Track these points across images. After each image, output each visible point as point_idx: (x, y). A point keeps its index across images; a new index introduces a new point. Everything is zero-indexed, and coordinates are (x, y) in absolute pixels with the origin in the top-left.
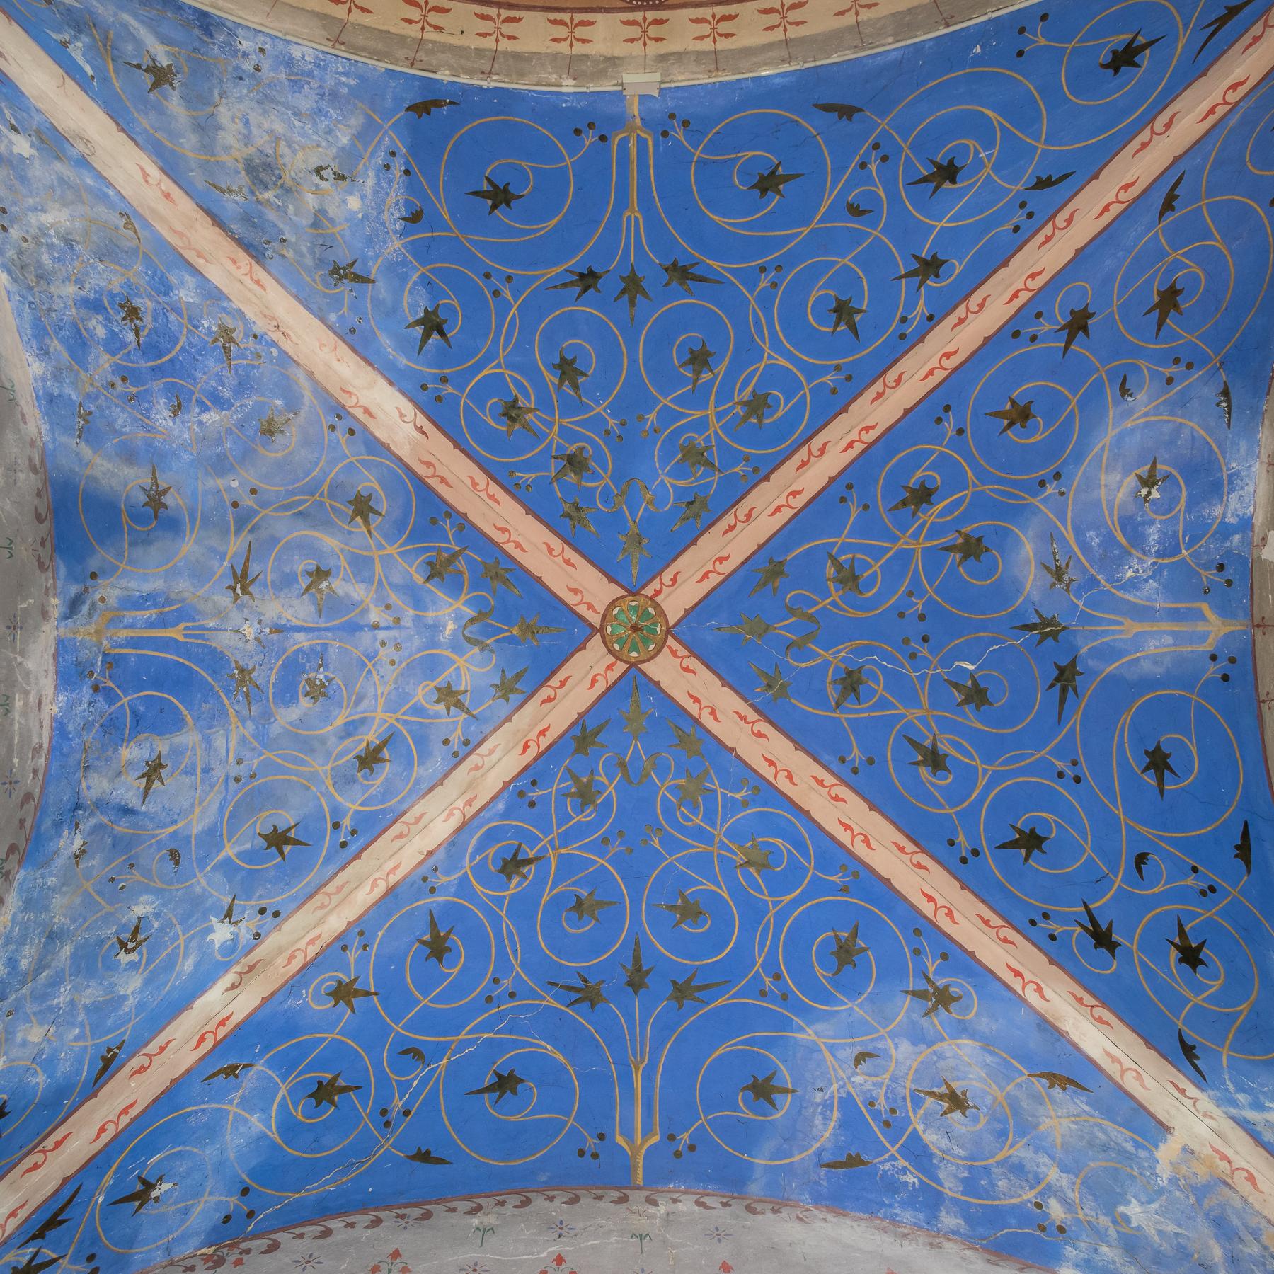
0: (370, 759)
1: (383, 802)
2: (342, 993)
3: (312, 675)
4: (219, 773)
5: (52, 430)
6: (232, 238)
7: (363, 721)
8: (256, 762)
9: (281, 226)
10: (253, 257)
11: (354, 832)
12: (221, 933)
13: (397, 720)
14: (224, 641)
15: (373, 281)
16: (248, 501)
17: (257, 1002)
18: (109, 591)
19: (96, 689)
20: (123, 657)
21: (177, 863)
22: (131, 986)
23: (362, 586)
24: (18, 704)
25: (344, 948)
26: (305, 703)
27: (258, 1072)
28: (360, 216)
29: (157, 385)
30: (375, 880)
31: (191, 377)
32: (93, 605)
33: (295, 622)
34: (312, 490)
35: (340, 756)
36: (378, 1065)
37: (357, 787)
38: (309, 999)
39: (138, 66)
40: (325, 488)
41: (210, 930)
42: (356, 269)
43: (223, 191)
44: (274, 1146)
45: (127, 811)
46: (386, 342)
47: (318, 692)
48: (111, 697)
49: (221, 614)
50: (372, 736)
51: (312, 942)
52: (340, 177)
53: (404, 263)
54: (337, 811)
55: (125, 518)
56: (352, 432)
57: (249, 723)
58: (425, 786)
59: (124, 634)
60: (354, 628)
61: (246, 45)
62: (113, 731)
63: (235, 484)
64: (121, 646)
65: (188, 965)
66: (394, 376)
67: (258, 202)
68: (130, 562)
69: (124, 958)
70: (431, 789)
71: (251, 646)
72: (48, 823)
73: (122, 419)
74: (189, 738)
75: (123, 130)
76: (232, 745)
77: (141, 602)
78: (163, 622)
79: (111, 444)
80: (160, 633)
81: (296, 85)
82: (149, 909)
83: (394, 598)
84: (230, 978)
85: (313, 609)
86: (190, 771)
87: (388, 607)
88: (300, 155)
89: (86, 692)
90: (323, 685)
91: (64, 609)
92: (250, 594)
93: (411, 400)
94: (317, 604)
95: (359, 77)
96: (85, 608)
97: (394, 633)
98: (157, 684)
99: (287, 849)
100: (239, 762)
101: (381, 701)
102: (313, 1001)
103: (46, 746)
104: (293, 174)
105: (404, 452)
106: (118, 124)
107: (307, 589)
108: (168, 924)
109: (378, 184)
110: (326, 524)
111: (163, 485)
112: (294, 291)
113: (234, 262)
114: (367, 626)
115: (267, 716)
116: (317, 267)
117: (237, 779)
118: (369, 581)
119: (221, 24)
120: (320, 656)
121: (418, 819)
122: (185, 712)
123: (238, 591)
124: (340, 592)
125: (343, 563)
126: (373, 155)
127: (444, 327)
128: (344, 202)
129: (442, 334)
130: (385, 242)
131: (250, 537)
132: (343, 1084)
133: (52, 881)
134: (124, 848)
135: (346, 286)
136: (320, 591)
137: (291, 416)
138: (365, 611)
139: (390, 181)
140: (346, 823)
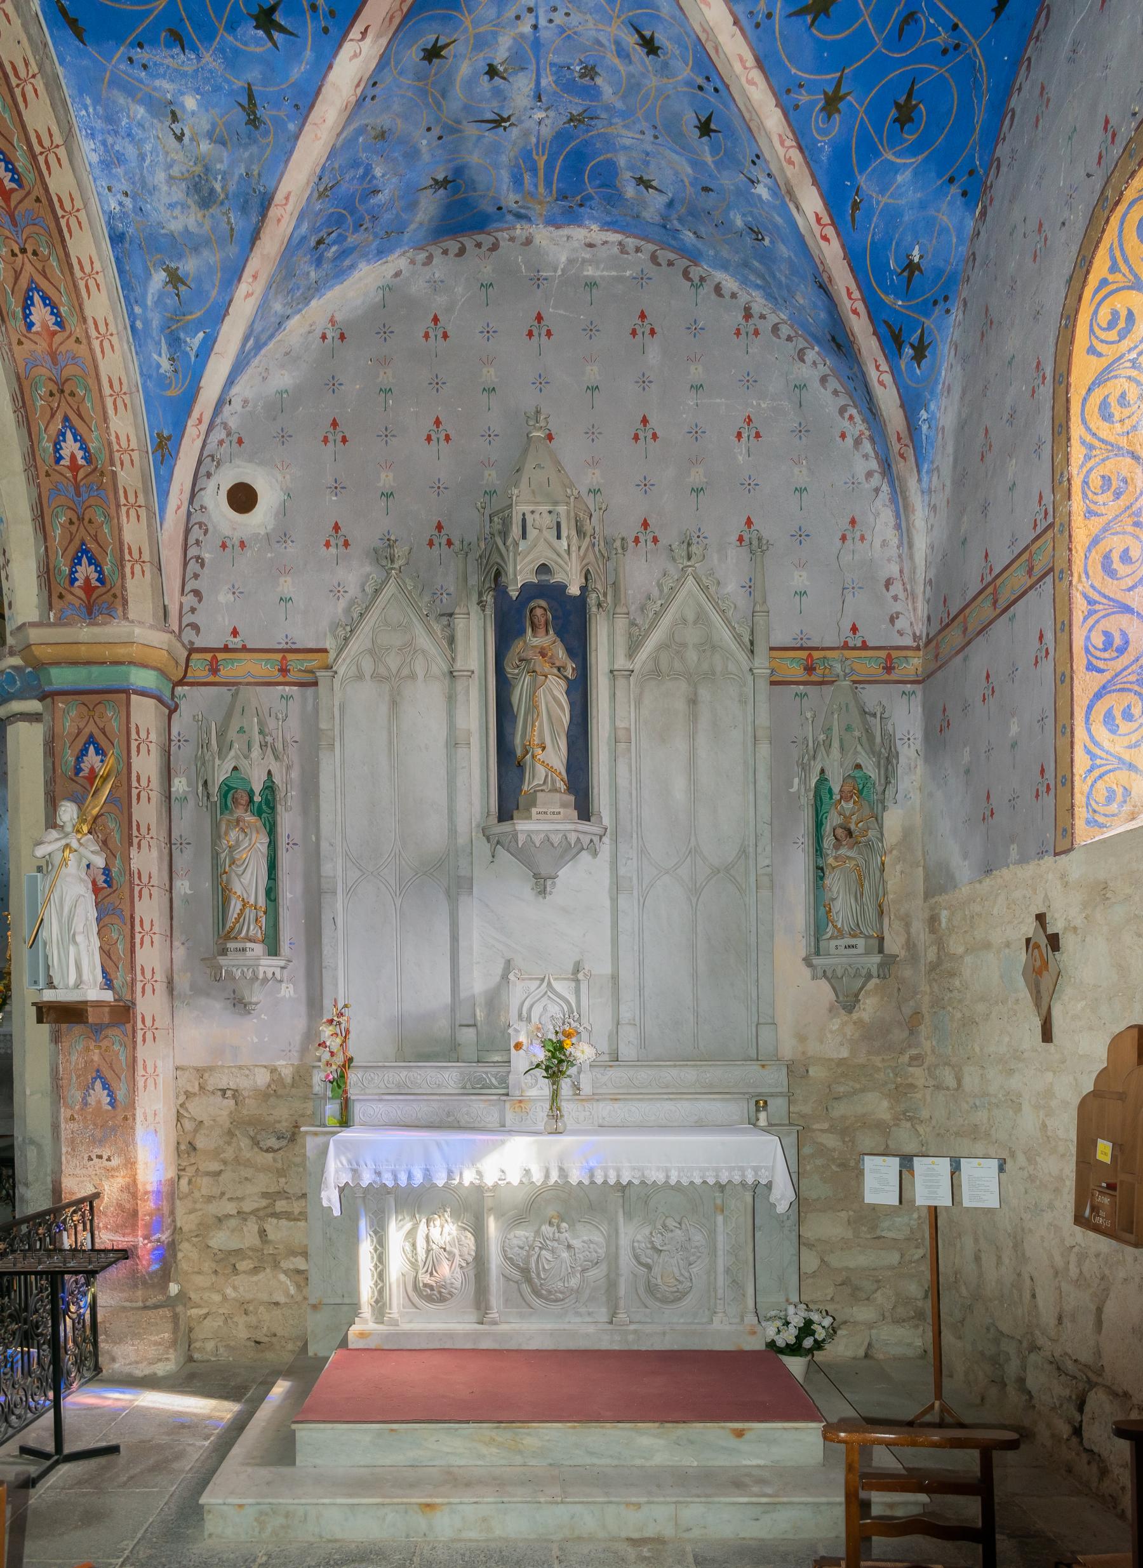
0: (650, 46)
1: (687, 48)
2: (832, 103)
3: (576, 75)
4: (649, 148)
5: (400, 246)
6: (263, 221)
7: (618, 43)
8: (644, 123)
9: (236, 177)
10: (270, 204)
11: (708, 79)
12: (762, 191)
13: (618, 17)
14: (547, 132)
15: (249, 84)
16: (436, 131)
17: (814, 189)
18: (510, 199)
19: (581, 205)
20: (558, 190)
21: (712, 190)
22: (784, 251)
23: (500, 39)
24: (590, 271)
25: (796, 107)
26: (599, 81)
27: (866, 181)
28: (198, 97)
29: (362, 208)
30: (748, 81)
31: (353, 195)
32: (520, 207)
33: (532, 85)
34: (423, 92)
35: (646, 67)
36: (904, 62)
37: (672, 63)
38: (826, 139)
39: (177, 295)
40: (421, 84)
41: (759, 197)
42: (245, 101)
43: (232, 229)
44: (926, 160)
45: (670, 204)
46: (297, 72)
47: (590, 72)
48: (589, 197)
49: (526, 134)
50: (630, 40)
51: (782, 143)
52: (175, 118)
53: (222, 51)
54: (689, 83)
55: (457, 197)
56: (375, 84)
57: (614, 120)
58: (678, 13)
59: (541, 189)
60: (537, 44)
61: (113, 204)
62: (613, 198)
63: (424, 142)
64: (551, 192)
65: (779, 220)
66: (324, 64)
67: (227, 198)
68: (488, 189)
69: (767, 242)
70: (681, 9)
71: (552, 114)
72: (673, 242)
73: (387, 216)
74: (622, 161)
75: (227, 310)
76: (631, 135)
77: (517, 181)
78: (534, 170)
79: (404, 216)
80: (541, 173)
81: (120, 159)
82: (738, 216)
83: (511, 13)
84: (792, 206)
85: (521, 74)
86: (647, 164)
87: (518, 18)
88: (173, 155)
89: (582, 210)
90: (585, 68)
91: (523, 222)
92: (509, 117)
93: (340, 46)
94: (515, 73)
95: (81, 95)
96: (523, 211)
97: (541, 12)
98: (580, 173)
99: (713, 126)
100: (643, 133)
101: (601, 27)
102: (825, 138)
103: (618, 237)
104: (191, 163)
105: (384, 41)
106: (225, 316)
107: (504, 79)
108: (751, 213)
109: (164, 76)
110: (450, 77)
111: (431, 182)
112: (282, 165)
113: (279, 221)
114: (535, 34)
115: (608, 108)
116: (255, 141)
117: (656, 137)
118: (495, 34)
119: (112, 228)
120: (561, 69)
121: (704, 30)
122: (602, 158)
123: (507, 124)
124: (507, 55)
125: (481, 55)
126: (141, 82)
127: (266, 7)
128: (193, 113)
129: (273, 9)
130: (211, 71)
131: (465, 123)
132: (904, 97)
133: (711, 253)
134: (694, 214)
135: (262, 113)
136: (506, 70)
137: (369, 128)
138: (522, 36)
139: (155, 64)
140: (700, 81)
